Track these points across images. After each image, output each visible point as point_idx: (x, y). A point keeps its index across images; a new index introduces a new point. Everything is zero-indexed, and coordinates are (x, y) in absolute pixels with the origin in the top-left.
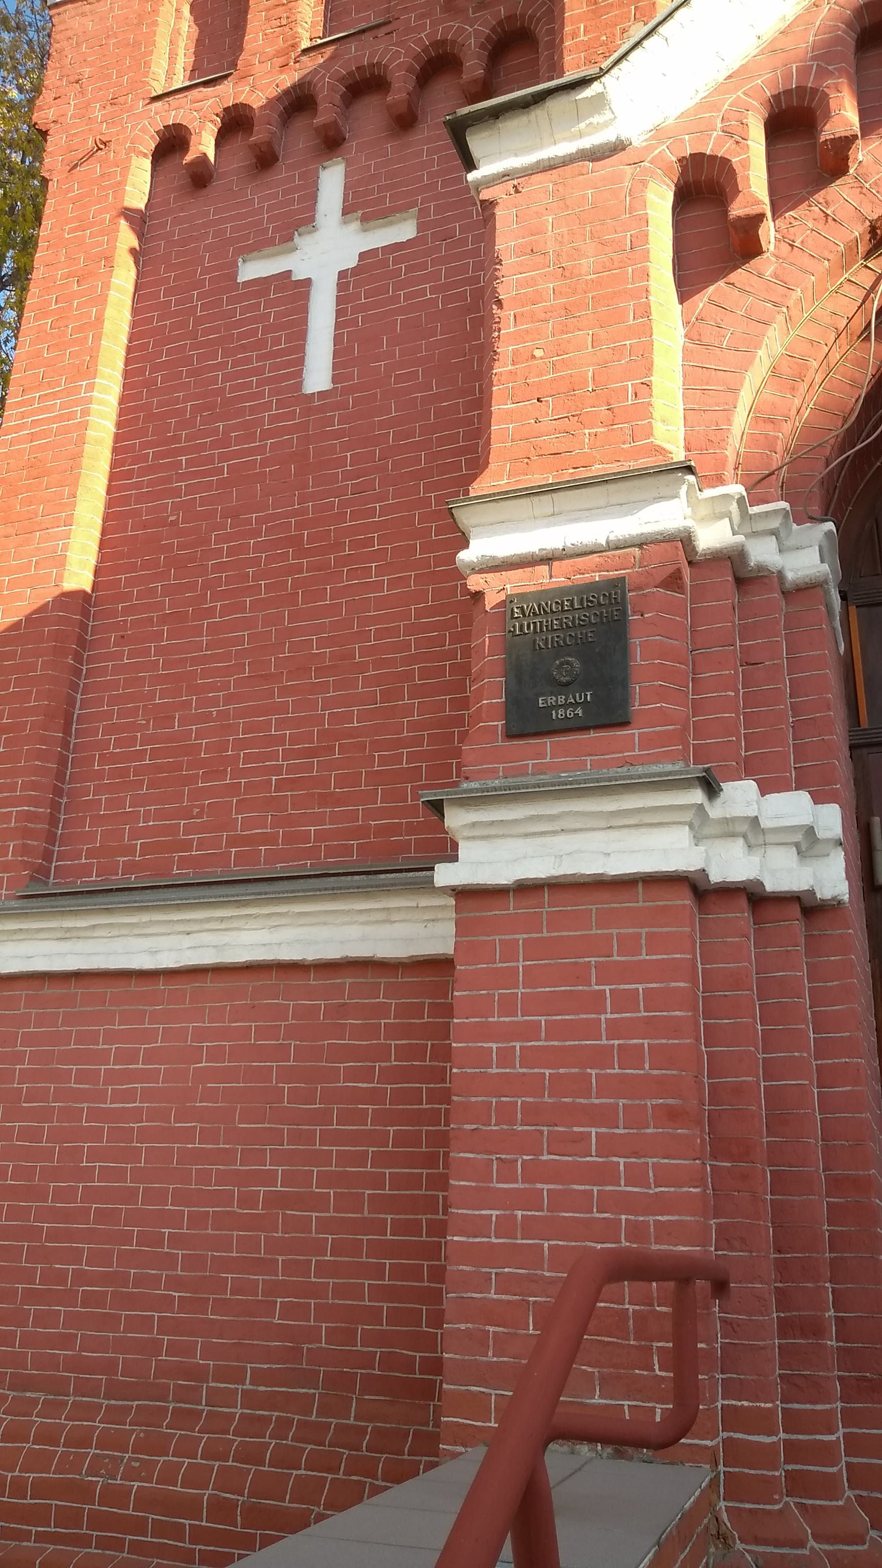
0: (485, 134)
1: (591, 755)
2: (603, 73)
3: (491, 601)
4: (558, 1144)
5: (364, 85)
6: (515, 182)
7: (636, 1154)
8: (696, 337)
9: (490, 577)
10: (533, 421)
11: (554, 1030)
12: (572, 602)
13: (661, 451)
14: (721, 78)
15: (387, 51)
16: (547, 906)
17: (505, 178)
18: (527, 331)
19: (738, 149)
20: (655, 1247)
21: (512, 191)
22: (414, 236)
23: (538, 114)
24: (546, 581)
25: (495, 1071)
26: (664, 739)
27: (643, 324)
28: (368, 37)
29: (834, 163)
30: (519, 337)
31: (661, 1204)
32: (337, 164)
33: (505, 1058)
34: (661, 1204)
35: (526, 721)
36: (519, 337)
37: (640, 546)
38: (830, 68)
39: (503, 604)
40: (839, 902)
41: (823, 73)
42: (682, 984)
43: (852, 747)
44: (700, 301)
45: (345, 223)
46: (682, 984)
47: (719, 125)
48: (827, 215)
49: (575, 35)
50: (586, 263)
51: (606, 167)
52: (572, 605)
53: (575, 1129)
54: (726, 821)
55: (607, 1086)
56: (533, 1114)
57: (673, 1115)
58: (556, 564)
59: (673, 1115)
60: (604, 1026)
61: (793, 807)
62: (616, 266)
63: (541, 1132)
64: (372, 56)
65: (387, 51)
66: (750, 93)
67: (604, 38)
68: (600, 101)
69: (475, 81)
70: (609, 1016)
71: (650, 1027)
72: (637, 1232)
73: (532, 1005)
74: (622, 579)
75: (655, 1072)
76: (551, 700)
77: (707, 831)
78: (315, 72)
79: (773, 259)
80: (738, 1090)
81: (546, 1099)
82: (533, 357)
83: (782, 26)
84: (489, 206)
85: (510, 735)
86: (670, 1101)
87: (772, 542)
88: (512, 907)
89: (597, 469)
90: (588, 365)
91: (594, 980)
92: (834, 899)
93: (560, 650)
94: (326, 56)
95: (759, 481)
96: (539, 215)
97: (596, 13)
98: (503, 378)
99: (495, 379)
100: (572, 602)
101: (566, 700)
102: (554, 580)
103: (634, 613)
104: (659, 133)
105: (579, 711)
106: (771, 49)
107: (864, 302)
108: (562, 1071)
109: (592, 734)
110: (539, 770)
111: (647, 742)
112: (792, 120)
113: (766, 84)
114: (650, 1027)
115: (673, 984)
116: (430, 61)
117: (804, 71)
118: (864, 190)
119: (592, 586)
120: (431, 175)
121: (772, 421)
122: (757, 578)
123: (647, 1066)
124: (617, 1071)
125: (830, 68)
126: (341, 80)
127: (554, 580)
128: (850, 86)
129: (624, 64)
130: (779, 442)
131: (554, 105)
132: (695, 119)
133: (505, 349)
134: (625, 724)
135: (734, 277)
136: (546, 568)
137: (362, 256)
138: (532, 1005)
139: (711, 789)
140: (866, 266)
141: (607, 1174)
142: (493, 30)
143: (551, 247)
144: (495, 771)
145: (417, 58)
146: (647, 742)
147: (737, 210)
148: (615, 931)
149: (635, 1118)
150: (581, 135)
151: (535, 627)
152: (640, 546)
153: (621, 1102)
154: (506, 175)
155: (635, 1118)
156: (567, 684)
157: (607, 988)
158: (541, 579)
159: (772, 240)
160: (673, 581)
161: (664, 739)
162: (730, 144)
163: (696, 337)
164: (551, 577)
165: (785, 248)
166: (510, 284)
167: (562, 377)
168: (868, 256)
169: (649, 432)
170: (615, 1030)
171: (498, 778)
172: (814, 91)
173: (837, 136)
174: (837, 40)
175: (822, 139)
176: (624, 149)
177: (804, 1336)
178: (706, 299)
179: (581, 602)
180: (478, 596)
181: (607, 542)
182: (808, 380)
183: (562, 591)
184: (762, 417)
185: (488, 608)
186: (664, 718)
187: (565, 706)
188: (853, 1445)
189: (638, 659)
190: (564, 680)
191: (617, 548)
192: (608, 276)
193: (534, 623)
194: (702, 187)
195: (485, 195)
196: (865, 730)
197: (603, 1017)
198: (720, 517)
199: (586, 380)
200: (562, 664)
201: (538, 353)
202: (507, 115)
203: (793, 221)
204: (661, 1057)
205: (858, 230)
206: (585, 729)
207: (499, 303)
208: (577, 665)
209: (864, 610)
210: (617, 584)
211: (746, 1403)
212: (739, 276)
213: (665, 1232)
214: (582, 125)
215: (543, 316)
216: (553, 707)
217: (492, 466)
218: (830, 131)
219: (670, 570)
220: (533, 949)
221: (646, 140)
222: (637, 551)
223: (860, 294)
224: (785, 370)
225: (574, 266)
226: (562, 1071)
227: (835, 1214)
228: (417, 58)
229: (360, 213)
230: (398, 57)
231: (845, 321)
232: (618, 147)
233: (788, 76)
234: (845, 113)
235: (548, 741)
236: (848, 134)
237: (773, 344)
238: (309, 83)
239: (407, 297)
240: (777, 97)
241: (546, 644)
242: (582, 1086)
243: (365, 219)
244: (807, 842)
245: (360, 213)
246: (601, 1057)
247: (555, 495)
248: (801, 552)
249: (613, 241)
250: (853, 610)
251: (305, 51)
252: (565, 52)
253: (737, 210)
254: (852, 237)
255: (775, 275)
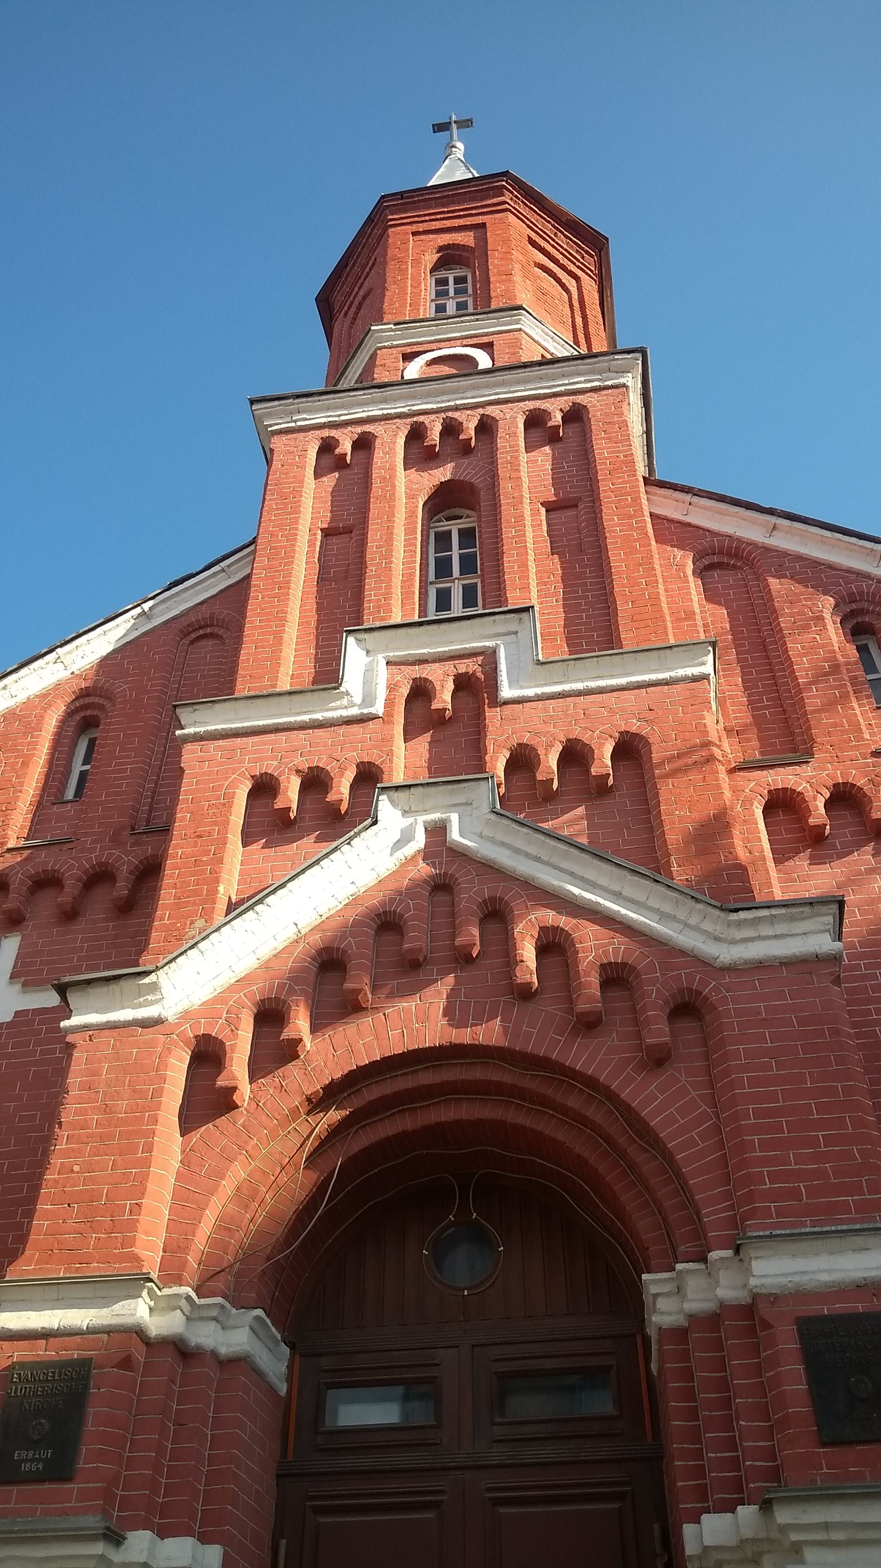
0: (79, 994)
1: (42, 1504)
2: (157, 969)
5: (44, 882)
6: (91, 1033)
8: (187, 1164)
13: (137, 1259)
14: (233, 981)
15: (66, 862)
18: (72, 1149)
23: (114, 987)
27: (146, 1158)
28: (56, 849)
30: (67, 1154)
32: (17, 936)
36: (67, 1154)
41: (291, 991)
43: (279, 1476)
44: (195, 1137)
45: (11, 983)
47: (225, 1015)
48: (282, 1086)
49: (162, 919)
51: (149, 1035)
52: (53, 1376)
64: (55, 864)
65: (66, 862)
66: (248, 995)
67: (179, 925)
68: (154, 987)
74: (90, 1360)
76: (24, 1454)
78: (12, 867)
79: (245, 1112)
82: (72, 1171)
83: (275, 952)
87: (212, 1326)
94: (24, 857)
95: (212, 1276)
96: (100, 1061)
97: (178, 906)
101: (34, 1455)
104: (186, 1015)
105: (40, 1466)
106: (266, 966)
107: (301, 1146)
109: (47, 1486)
112: (270, 1016)
113: (257, 990)
117: (281, 986)
120: (80, 959)
121: (229, 1229)
126: (30, 877)
128: (306, 1001)
129: (173, 965)
131: (124, 984)
132: (210, 1007)
133: (56, 1161)
134: (68, 1479)
135: (218, 1121)
136: (45, 1342)
137: (17, 1014)
139: (115, 1538)
140: (307, 1120)
142: (141, 862)
145: (85, 872)
150: (140, 1006)
151: (25, 1392)
154: (86, 1027)
158: (41, 1352)
159: (247, 1099)
160: (126, 1363)
163: (187, 1164)
164: (46, 1350)
165: (254, 1105)
168: (308, 1113)
169: (132, 1242)
172: (284, 1002)
174: (304, 969)
178: (198, 1136)
179: (60, 1375)
181: (87, 1328)
182: (259, 1198)
184: (223, 1226)
187: (32, 1460)
189: (89, 1426)
190: (36, 1438)
193: (26, 1388)
194: (207, 1055)
195: (70, 1039)
196: (290, 1462)
198: (174, 1309)
200: (37, 1424)
201: (76, 1168)
206: (41, 1481)
212: (222, 1121)
214: (142, 999)
221: (178, 1018)
228: (85, 872)
229: (23, 979)
230: (72, 867)
231: (287, 1160)
232: (158, 1022)
233: (271, 988)
234: (300, 1023)
235: (15, 1489)
237: (238, 1172)
238: (7, 875)
239: (43, 1052)
240: (263, 1001)
241: (30, 1407)
243: (25, 985)
245: (23, 979)
247: (60, 1286)
248: (236, 1330)
249: (141, 1091)
251: (9, 850)
255: (243, 1126)
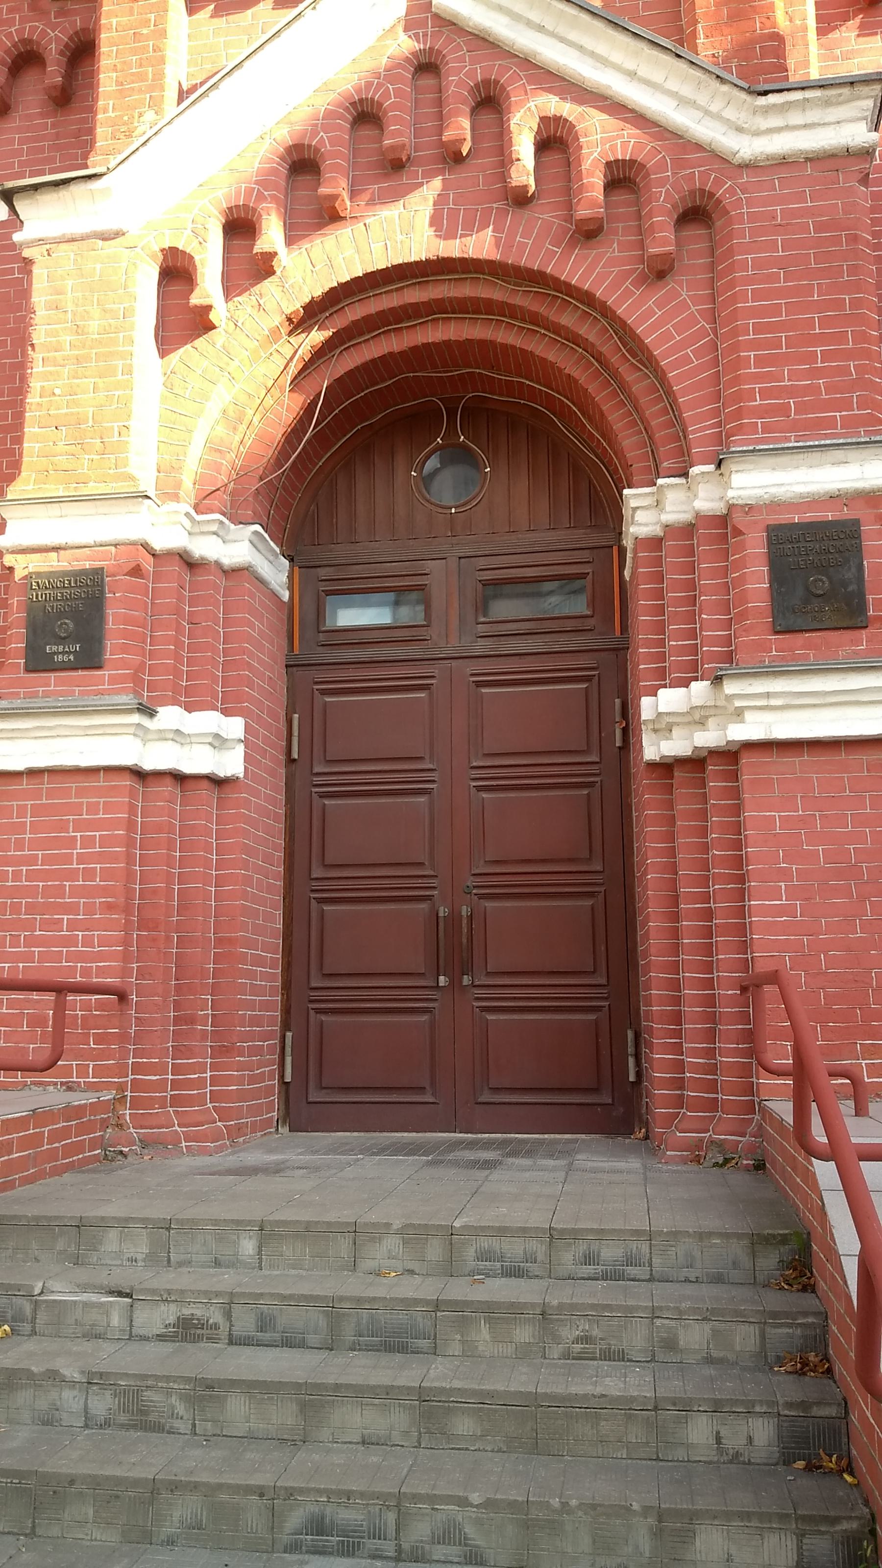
0: (27, 202)
3: (19, 574)
4: (46, 925)
6: (48, 246)
7: (87, 930)
8: (169, 386)
9: (19, 557)
10: (51, 444)
11: (46, 860)
12: (70, 581)
16: (46, 784)
17: (41, 242)
18: (51, 373)
19: (200, 249)
20: (95, 980)
21: (46, 253)
22: (6, 218)
23: (63, 193)
24: (55, 564)
25: (10, 884)
26: (122, 679)
29: (264, 268)
30: (46, 377)
31: (100, 957)
33: (17, 876)
34: (100, 957)
35: (38, 662)
36: (46, 377)
37: (116, 545)
38: (266, 193)
39: (25, 578)
40: (237, 778)
41: (260, 197)
42: (121, 832)
44: (174, 358)
46: (121, 832)
48: (260, 305)
49: (105, 111)
50: (94, 326)
52: (70, 584)
53: (56, 917)
54: (160, 731)
55: (75, 892)
56: (31, 908)
57: (109, 907)
58: (62, 552)
59: (109, 907)
60: (75, 857)
61: (209, 721)
62: (113, 330)
63: (36, 919)
69: (55, 87)
70: (79, 851)
71: (100, 857)
72: (86, 972)
73: (35, 844)
75: (102, 883)
76: (55, 648)
77: (150, 737)
80: (155, 891)
81: (40, 900)
82: (54, 394)
84: (28, 263)
85: (28, 670)
86: (109, 900)
88: (25, 784)
89: (92, 488)
90: (90, 407)
91: (71, 830)
92: (233, 776)
93: (61, 614)
98: (33, 407)
99: (28, 407)
100: (70, 581)
102: (60, 564)
103: (110, 592)
105: (72, 657)
108: (49, 883)
109: (80, 673)
110: (46, 695)
111: (113, 680)
114: (100, 857)
115: (116, 832)
116: (20, 55)
117: (249, 192)
118: (285, 290)
119: (84, 572)
121: (220, 451)
122: (201, 564)
123: (98, 880)
124: (81, 883)
125: (266, 193)
127: (60, 564)
128: (278, 209)
130: (224, 468)
131: (76, 189)
133: (35, 385)
134: (99, 668)
136: (56, 554)
138: (35, 844)
141: (71, 941)
142: (71, 38)
143: (70, 307)
144: (18, 694)
146: (113, 680)
147: (195, 300)
148: (85, 800)
149: (89, 909)
152: (116, 545)
153: (82, 900)
155: (89, 909)
156: (64, 638)
157: (79, 834)
161: (122, 679)
162: (195, 243)
163: (169, 386)
166: (39, 335)
167: (72, 414)
168: (290, 333)
170: (81, 859)
171: (20, 698)
173: (264, 251)
174: (273, 171)
175: (254, 252)
176: (123, 234)
177: (186, 1024)
179: (76, 582)
180: (11, 569)
183: (65, 574)
185: (16, 580)
186: (124, 664)
187: (63, 653)
188: (214, 1081)
189: (110, 625)
190: (63, 635)
191: (101, 546)
192: (107, 338)
194: (176, 272)
195: (26, 253)
197: (75, 851)
199: (88, 418)
200: (62, 624)
201: (57, 391)
202: (43, 189)
203: (238, 305)
204: (107, 874)
205: (277, 320)
206: (76, 669)
207: (32, 345)
208: (71, 626)
209: (304, 570)
210: (98, 573)
211: (145, 1060)
213: (101, 972)
215: (62, 362)
216: (55, 653)
217: (23, 474)
218: (262, 245)
219: (133, 565)
220: (37, 811)
222: (113, 548)
223: (282, 363)
224: (231, 413)
225: (84, 326)
226: (49, 883)
227: (217, 959)
233: (238, 194)
236: (271, 250)
237: (222, 396)
240: (230, 209)
241: (53, 609)
242: (59, 891)
244: (218, 742)
246: (72, 875)
250: (296, 569)
252: (98, 125)
253: (195, 300)
254: (273, 325)
